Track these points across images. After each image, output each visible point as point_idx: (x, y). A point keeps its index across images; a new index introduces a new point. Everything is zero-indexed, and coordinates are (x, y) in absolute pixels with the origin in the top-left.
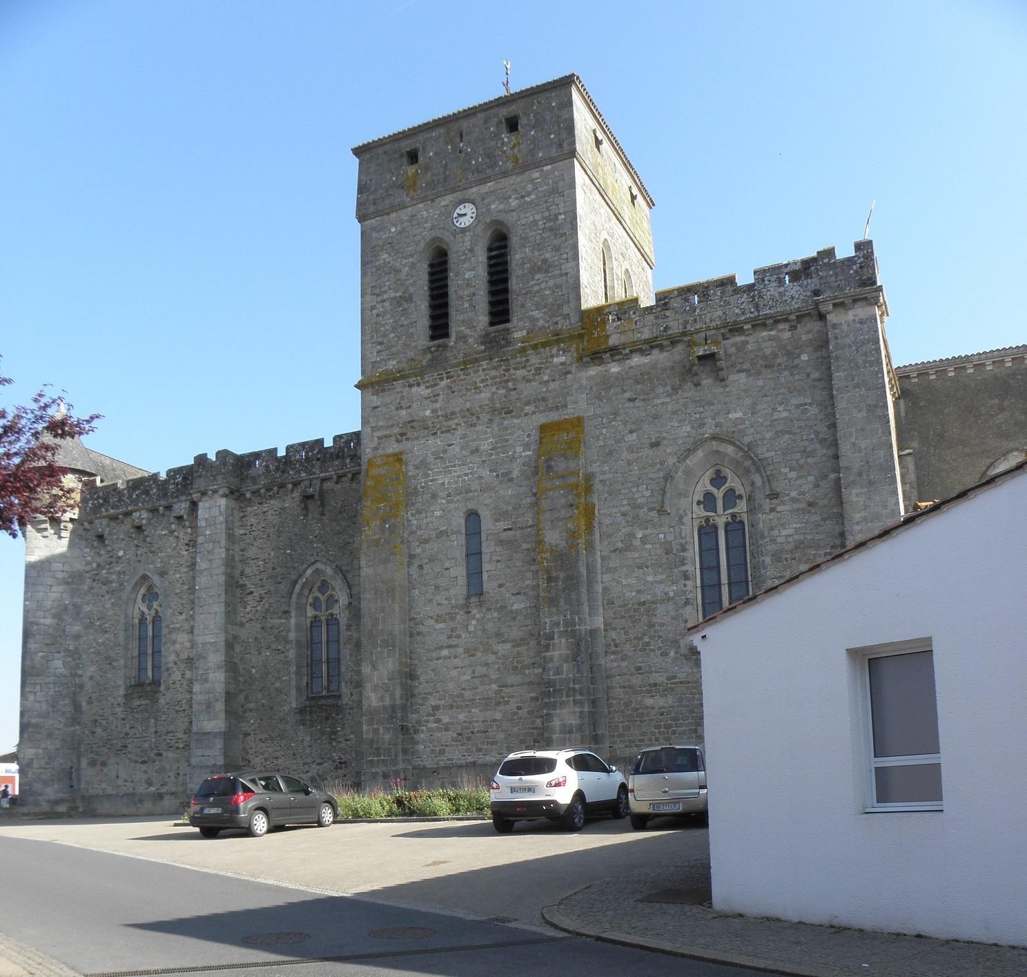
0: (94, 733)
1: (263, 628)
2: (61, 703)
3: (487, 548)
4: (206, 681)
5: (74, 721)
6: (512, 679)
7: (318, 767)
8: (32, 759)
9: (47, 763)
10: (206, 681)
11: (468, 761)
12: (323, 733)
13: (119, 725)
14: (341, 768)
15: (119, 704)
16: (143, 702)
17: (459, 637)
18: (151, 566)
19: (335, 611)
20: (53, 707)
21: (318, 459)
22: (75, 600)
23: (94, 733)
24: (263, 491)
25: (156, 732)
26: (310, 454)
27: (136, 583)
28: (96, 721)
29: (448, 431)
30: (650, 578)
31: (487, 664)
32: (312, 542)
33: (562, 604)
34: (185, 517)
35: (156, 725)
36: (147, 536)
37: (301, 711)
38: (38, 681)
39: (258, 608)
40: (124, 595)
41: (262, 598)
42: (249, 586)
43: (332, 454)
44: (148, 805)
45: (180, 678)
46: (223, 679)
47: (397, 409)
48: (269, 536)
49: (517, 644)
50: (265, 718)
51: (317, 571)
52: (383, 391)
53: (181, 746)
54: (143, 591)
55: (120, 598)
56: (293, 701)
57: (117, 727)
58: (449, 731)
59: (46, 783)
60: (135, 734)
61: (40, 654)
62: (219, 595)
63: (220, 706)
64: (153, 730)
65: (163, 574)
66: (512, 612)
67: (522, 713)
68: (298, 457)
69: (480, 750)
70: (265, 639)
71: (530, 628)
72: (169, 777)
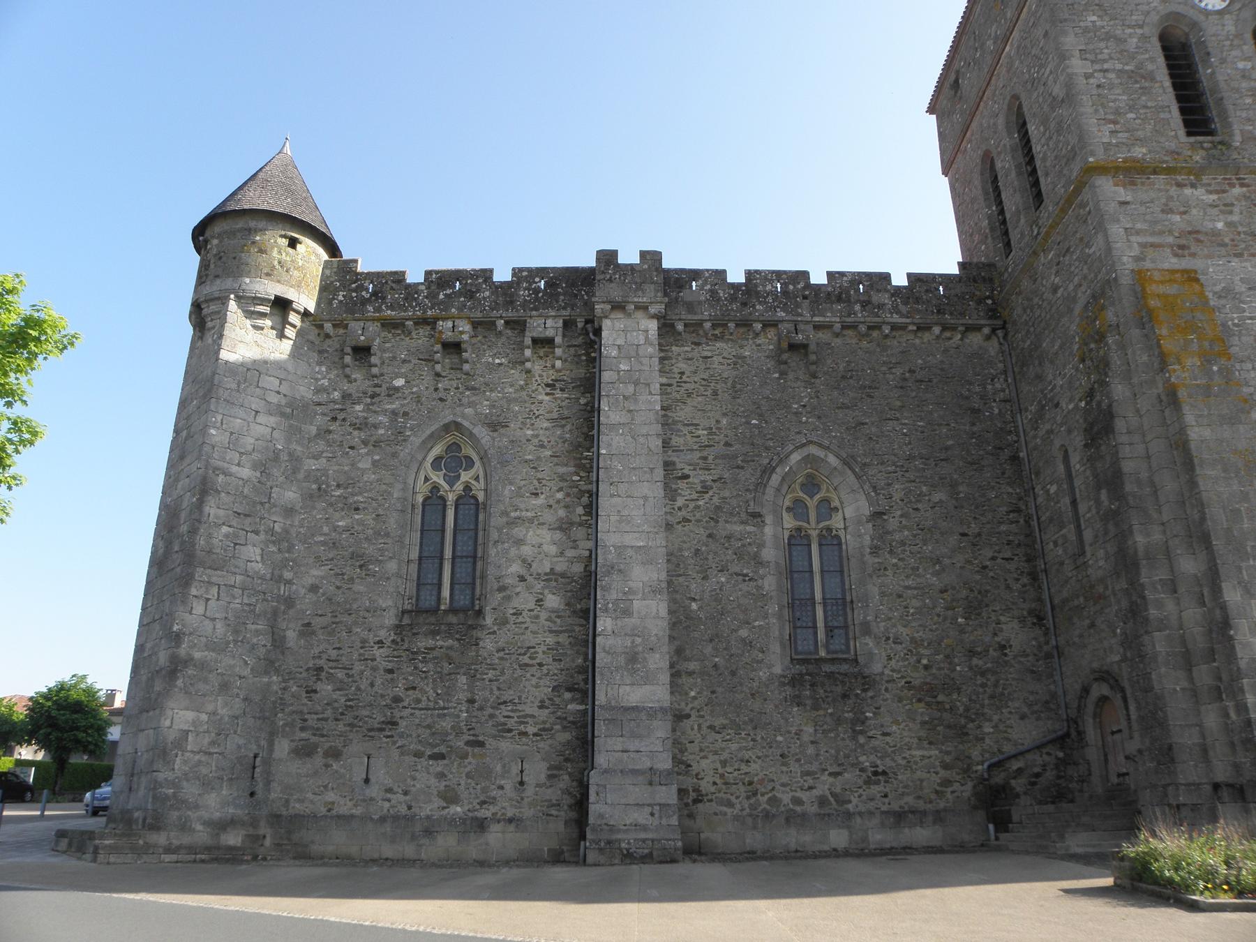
0: (315, 691)
1: (710, 536)
2: (251, 627)
4: (627, 613)
5: (269, 665)
7: (831, 779)
8: (187, 732)
9: (213, 743)
10: (627, 613)
12: (839, 721)
13: (378, 682)
14: (877, 783)
15: (380, 642)
16: (440, 643)
18: (469, 411)
19: (836, 522)
20: (236, 632)
21: (805, 297)
22: (293, 446)
23: (315, 691)
24: (708, 325)
25: (471, 701)
26: (791, 287)
27: (431, 436)
28: (320, 669)
34: (558, 340)
35: (471, 689)
36: (467, 362)
37: (795, 681)
38: (214, 579)
39: (701, 503)
40: (404, 452)
41: (705, 489)
42: (679, 466)
44: (446, 843)
45: (532, 605)
46: (663, 612)
47: (1163, 211)
48: (715, 393)
50: (720, 690)
52: (1133, 183)
53: (531, 730)
54: (437, 450)
55: (394, 455)
56: (776, 663)
57: (372, 685)
59: (207, 785)
60: (418, 701)
61: (225, 529)
62: (652, 470)
63: (658, 661)
64: (463, 696)
65: (495, 426)
68: (769, 287)
70: (715, 553)
72: (501, 787)
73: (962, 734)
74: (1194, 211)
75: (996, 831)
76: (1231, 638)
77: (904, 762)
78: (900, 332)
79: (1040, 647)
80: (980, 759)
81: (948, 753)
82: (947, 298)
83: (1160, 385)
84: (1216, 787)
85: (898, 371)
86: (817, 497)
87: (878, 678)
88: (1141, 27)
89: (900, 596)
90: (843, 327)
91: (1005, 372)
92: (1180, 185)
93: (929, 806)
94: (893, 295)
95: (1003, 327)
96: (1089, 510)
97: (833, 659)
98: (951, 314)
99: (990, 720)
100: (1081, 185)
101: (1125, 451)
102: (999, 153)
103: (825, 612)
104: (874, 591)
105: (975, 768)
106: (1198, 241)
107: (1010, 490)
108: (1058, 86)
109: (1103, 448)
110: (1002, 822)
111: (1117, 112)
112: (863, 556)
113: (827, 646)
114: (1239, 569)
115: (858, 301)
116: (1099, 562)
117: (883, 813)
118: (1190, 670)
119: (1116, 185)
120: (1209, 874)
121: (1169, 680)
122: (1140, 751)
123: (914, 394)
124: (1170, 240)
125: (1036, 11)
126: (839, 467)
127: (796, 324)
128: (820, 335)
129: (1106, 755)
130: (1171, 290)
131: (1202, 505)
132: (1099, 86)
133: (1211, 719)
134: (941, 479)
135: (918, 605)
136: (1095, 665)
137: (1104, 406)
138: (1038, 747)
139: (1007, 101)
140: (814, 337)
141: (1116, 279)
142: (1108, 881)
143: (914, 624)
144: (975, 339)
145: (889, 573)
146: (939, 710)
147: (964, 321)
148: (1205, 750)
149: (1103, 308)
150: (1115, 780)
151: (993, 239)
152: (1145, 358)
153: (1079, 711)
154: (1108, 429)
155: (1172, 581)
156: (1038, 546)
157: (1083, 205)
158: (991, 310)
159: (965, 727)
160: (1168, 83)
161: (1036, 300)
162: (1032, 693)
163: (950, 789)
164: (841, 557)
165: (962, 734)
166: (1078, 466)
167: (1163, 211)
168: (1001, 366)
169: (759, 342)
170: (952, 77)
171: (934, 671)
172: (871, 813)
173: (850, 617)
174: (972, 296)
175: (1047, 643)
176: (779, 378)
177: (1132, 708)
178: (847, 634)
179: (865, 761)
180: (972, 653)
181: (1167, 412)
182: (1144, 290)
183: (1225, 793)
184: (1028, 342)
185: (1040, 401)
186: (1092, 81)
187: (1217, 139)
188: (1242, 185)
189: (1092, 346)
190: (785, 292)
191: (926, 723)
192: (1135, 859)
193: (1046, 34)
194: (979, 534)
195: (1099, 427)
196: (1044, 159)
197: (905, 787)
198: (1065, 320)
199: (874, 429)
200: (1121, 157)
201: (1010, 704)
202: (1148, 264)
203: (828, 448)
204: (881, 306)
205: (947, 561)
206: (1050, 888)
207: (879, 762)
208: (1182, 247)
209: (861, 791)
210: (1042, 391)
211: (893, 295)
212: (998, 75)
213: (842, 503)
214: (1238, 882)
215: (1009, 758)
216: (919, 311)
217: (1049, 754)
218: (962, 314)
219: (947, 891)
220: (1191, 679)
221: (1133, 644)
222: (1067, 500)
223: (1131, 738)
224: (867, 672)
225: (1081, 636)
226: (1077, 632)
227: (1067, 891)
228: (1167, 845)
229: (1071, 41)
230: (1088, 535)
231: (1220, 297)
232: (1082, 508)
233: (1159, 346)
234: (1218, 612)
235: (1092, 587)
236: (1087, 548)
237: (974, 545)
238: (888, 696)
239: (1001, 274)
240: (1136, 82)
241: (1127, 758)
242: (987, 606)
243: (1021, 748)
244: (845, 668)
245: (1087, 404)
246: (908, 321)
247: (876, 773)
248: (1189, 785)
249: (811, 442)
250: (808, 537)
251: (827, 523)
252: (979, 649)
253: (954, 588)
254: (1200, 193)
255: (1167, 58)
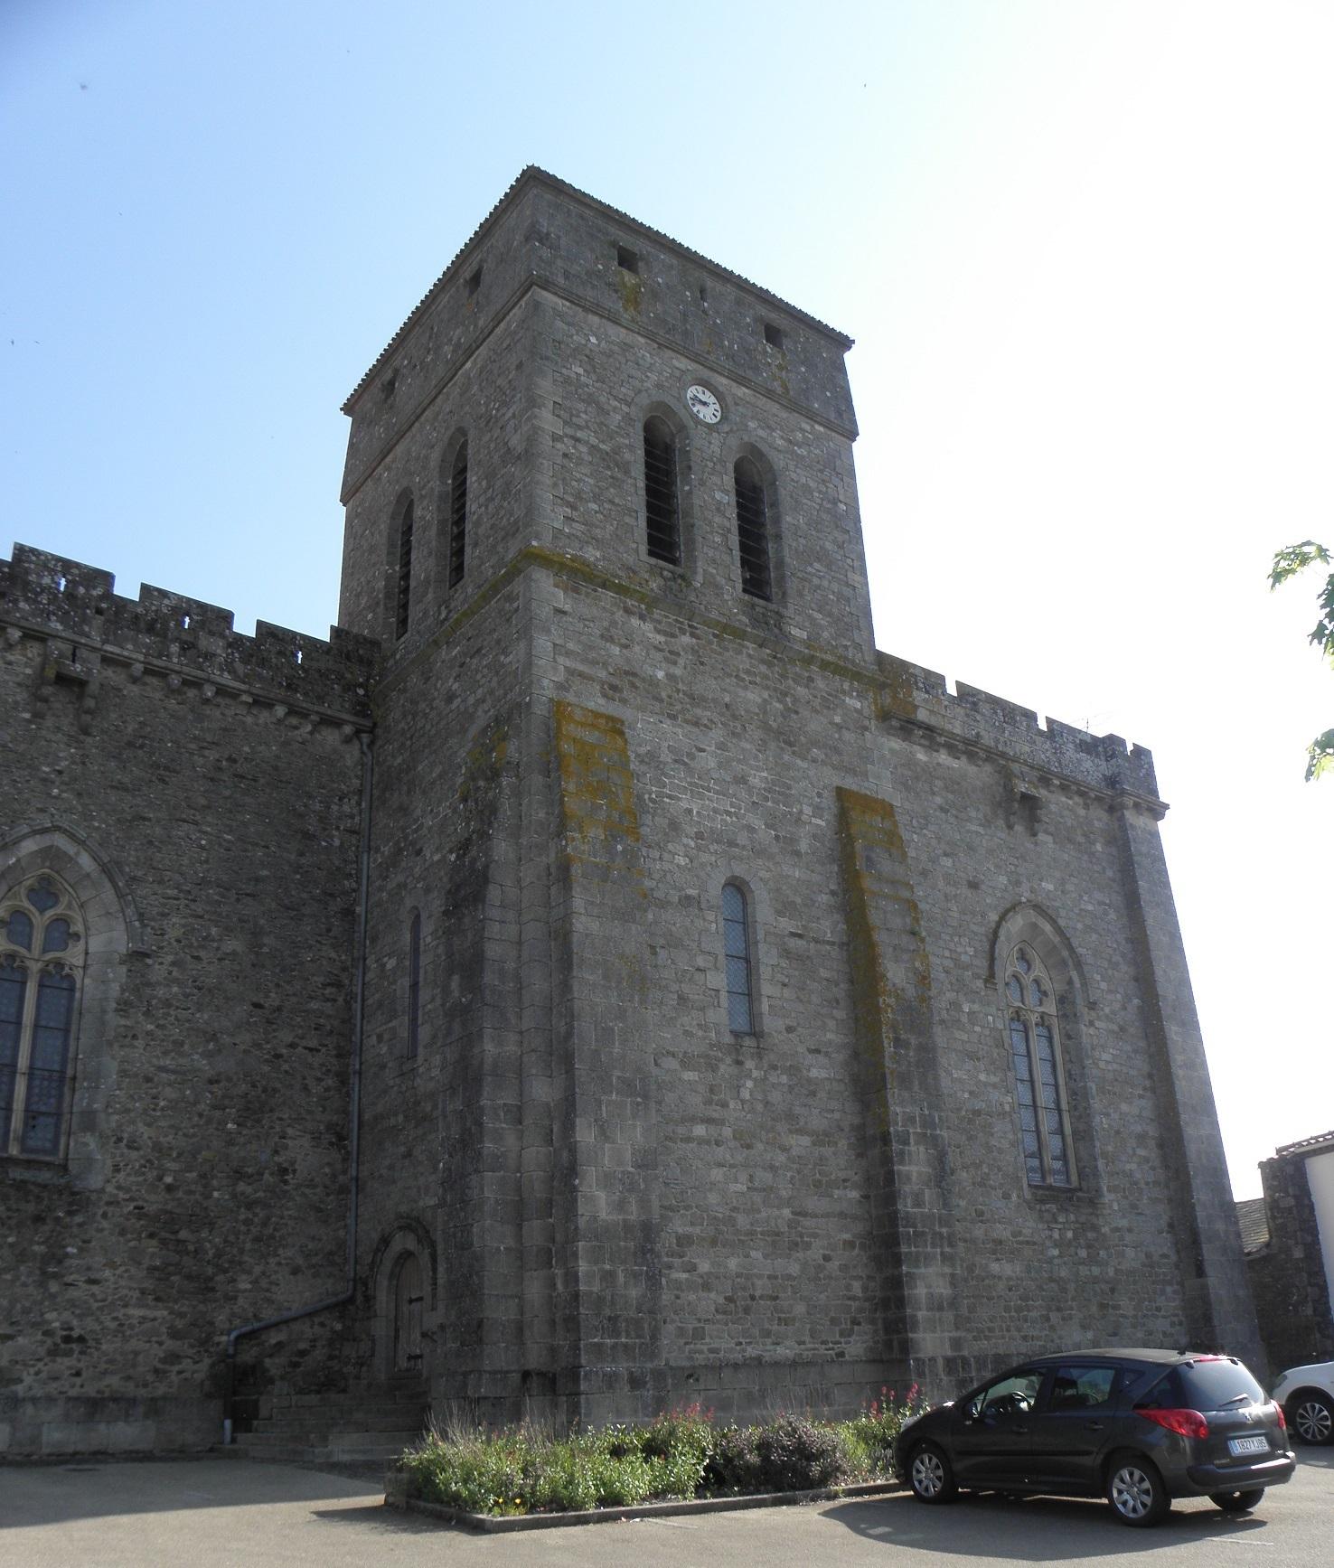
3: (767, 956)
6: (813, 1203)
11: (747, 1355)
14: (69, 1353)
17: (724, 1105)
19: (73, 956)
21: (99, 612)
26: (82, 590)
29: (696, 724)
30: (982, 1077)
31: (772, 1168)
32: (45, 781)
33: (916, 1088)
43: (137, 616)
47: (602, 636)
49: (822, 1138)
51: (49, 854)
52: (576, 590)
58: (709, 1290)
66: (809, 1080)
67: (833, 1266)
68: (46, 581)
69: (767, 1334)
71: (837, 1115)
73: (206, 1288)
74: (637, 648)
75: (235, 1429)
76: (574, 1189)
77: (113, 1325)
78: (228, 701)
79: (334, 1176)
80: (227, 1326)
81: (181, 1315)
82: (305, 671)
83: (553, 855)
84: (526, 1375)
85: (212, 755)
86: (50, 913)
87: (94, 1197)
88: (629, 405)
89: (148, 1080)
90: (147, 672)
91: (360, 792)
92: (627, 611)
93: (142, 1392)
94: (230, 645)
95: (371, 732)
96: (433, 999)
97: (29, 1162)
98: (306, 694)
99: (249, 1273)
100: (514, 572)
101: (494, 929)
102: (423, 497)
103: (29, 1088)
104: (112, 1067)
105: (216, 1339)
106: (633, 685)
107: (333, 955)
108: (517, 436)
109: (466, 920)
110: (243, 1417)
111: (579, 495)
112: (104, 1012)
113: (22, 1140)
114: (599, 1103)
115: (177, 639)
116: (433, 1069)
117: (69, 1399)
118: (520, 1226)
119: (556, 586)
120: (502, 1485)
121: (492, 1236)
122: (442, 1327)
123: (227, 793)
124: (602, 674)
125: (515, 333)
126: (94, 875)
127: (76, 646)
128: (109, 672)
129: (397, 1331)
130: (590, 736)
131: (572, 1016)
132: (565, 455)
133: (534, 1290)
134: (240, 920)
135: (174, 1096)
136: (403, 1209)
137: (479, 865)
138: (310, 1315)
139: (449, 433)
140: (101, 676)
141: (528, 705)
142: (378, 1499)
143: (162, 1124)
144: (331, 737)
145: (140, 1043)
146: (178, 1252)
147: (321, 710)
148: (520, 1329)
149: (505, 738)
150: (403, 1364)
151: (386, 609)
152: (542, 815)
153: (371, 1269)
154: (478, 898)
155: (519, 1108)
156: (356, 1039)
157: (510, 598)
158: (360, 703)
159: (211, 1279)
160: (642, 484)
161: (422, 705)
162: (313, 1238)
163: (177, 1368)
164: (69, 1010)
165: (206, 1288)
166: (429, 939)
167: (602, 636)
168: (356, 782)
169: (10, 657)
170: (388, 375)
171: (180, 1194)
172: (50, 1399)
173: (67, 1098)
174: (341, 677)
175: (345, 1172)
176: (29, 721)
177: (441, 1269)
178: (57, 1126)
179: (54, 1319)
180: (239, 1174)
181: (553, 890)
182: (559, 728)
183: (535, 1383)
184: (399, 760)
185: (398, 842)
186: (559, 446)
187: (679, 570)
188: (692, 635)
189: (481, 783)
190: (70, 595)
191: (156, 1268)
192: (417, 1468)
193: (520, 366)
194: (279, 1009)
195: (467, 891)
196: (478, 524)
197: (111, 1362)
198: (452, 741)
199: (158, 830)
200: (570, 552)
201: (281, 1251)
202: (570, 698)
203: (81, 843)
204: (209, 656)
205: (226, 1039)
206: (295, 1512)
207: (75, 1323)
208: (614, 688)
209: (40, 1365)
210: (403, 829)
211: (230, 645)
212: (448, 394)
213: (87, 929)
214: (533, 1493)
215: (267, 1328)
216: (260, 678)
217: (322, 1325)
218: (321, 699)
219: (152, 1517)
220: (519, 1237)
221: (456, 1185)
222: (405, 982)
223: (434, 1309)
224: (79, 1186)
225: (391, 1167)
226: (387, 1162)
227: (322, 1515)
228: (459, 1450)
229: (546, 387)
230: (424, 1033)
231: (642, 762)
232: (424, 995)
233: (562, 803)
234: (565, 1154)
235: (417, 1103)
236: (421, 1050)
237: (269, 1022)
238: (105, 1224)
239: (385, 659)
240: (609, 468)
241: (424, 1335)
242: (271, 1111)
243: (286, 1314)
244: (45, 1176)
245: (458, 857)
246: (243, 687)
247: (67, 1339)
248: (495, 1372)
249: (58, 828)
250: (24, 970)
251: (58, 954)
252: (250, 1170)
253: (229, 1079)
254: (647, 627)
255: (648, 453)
